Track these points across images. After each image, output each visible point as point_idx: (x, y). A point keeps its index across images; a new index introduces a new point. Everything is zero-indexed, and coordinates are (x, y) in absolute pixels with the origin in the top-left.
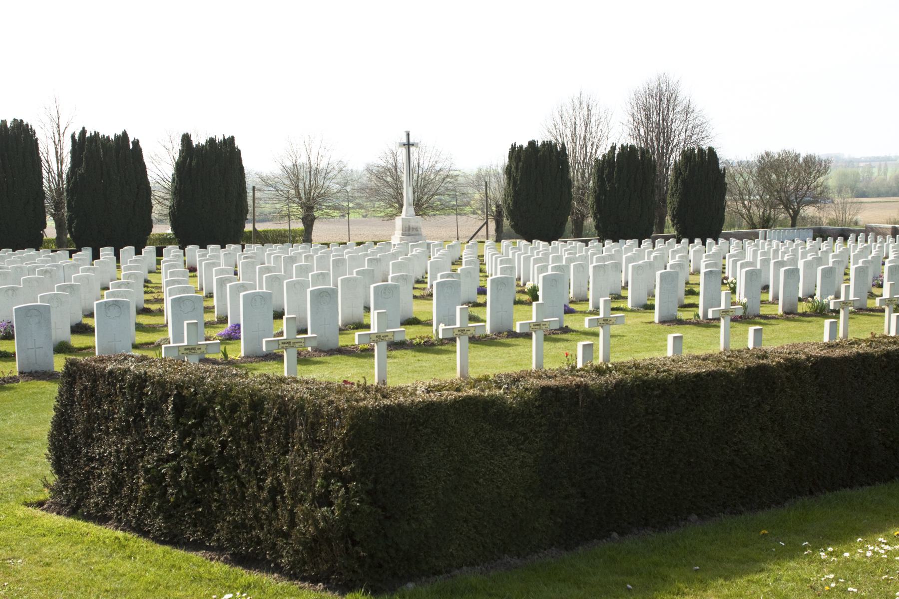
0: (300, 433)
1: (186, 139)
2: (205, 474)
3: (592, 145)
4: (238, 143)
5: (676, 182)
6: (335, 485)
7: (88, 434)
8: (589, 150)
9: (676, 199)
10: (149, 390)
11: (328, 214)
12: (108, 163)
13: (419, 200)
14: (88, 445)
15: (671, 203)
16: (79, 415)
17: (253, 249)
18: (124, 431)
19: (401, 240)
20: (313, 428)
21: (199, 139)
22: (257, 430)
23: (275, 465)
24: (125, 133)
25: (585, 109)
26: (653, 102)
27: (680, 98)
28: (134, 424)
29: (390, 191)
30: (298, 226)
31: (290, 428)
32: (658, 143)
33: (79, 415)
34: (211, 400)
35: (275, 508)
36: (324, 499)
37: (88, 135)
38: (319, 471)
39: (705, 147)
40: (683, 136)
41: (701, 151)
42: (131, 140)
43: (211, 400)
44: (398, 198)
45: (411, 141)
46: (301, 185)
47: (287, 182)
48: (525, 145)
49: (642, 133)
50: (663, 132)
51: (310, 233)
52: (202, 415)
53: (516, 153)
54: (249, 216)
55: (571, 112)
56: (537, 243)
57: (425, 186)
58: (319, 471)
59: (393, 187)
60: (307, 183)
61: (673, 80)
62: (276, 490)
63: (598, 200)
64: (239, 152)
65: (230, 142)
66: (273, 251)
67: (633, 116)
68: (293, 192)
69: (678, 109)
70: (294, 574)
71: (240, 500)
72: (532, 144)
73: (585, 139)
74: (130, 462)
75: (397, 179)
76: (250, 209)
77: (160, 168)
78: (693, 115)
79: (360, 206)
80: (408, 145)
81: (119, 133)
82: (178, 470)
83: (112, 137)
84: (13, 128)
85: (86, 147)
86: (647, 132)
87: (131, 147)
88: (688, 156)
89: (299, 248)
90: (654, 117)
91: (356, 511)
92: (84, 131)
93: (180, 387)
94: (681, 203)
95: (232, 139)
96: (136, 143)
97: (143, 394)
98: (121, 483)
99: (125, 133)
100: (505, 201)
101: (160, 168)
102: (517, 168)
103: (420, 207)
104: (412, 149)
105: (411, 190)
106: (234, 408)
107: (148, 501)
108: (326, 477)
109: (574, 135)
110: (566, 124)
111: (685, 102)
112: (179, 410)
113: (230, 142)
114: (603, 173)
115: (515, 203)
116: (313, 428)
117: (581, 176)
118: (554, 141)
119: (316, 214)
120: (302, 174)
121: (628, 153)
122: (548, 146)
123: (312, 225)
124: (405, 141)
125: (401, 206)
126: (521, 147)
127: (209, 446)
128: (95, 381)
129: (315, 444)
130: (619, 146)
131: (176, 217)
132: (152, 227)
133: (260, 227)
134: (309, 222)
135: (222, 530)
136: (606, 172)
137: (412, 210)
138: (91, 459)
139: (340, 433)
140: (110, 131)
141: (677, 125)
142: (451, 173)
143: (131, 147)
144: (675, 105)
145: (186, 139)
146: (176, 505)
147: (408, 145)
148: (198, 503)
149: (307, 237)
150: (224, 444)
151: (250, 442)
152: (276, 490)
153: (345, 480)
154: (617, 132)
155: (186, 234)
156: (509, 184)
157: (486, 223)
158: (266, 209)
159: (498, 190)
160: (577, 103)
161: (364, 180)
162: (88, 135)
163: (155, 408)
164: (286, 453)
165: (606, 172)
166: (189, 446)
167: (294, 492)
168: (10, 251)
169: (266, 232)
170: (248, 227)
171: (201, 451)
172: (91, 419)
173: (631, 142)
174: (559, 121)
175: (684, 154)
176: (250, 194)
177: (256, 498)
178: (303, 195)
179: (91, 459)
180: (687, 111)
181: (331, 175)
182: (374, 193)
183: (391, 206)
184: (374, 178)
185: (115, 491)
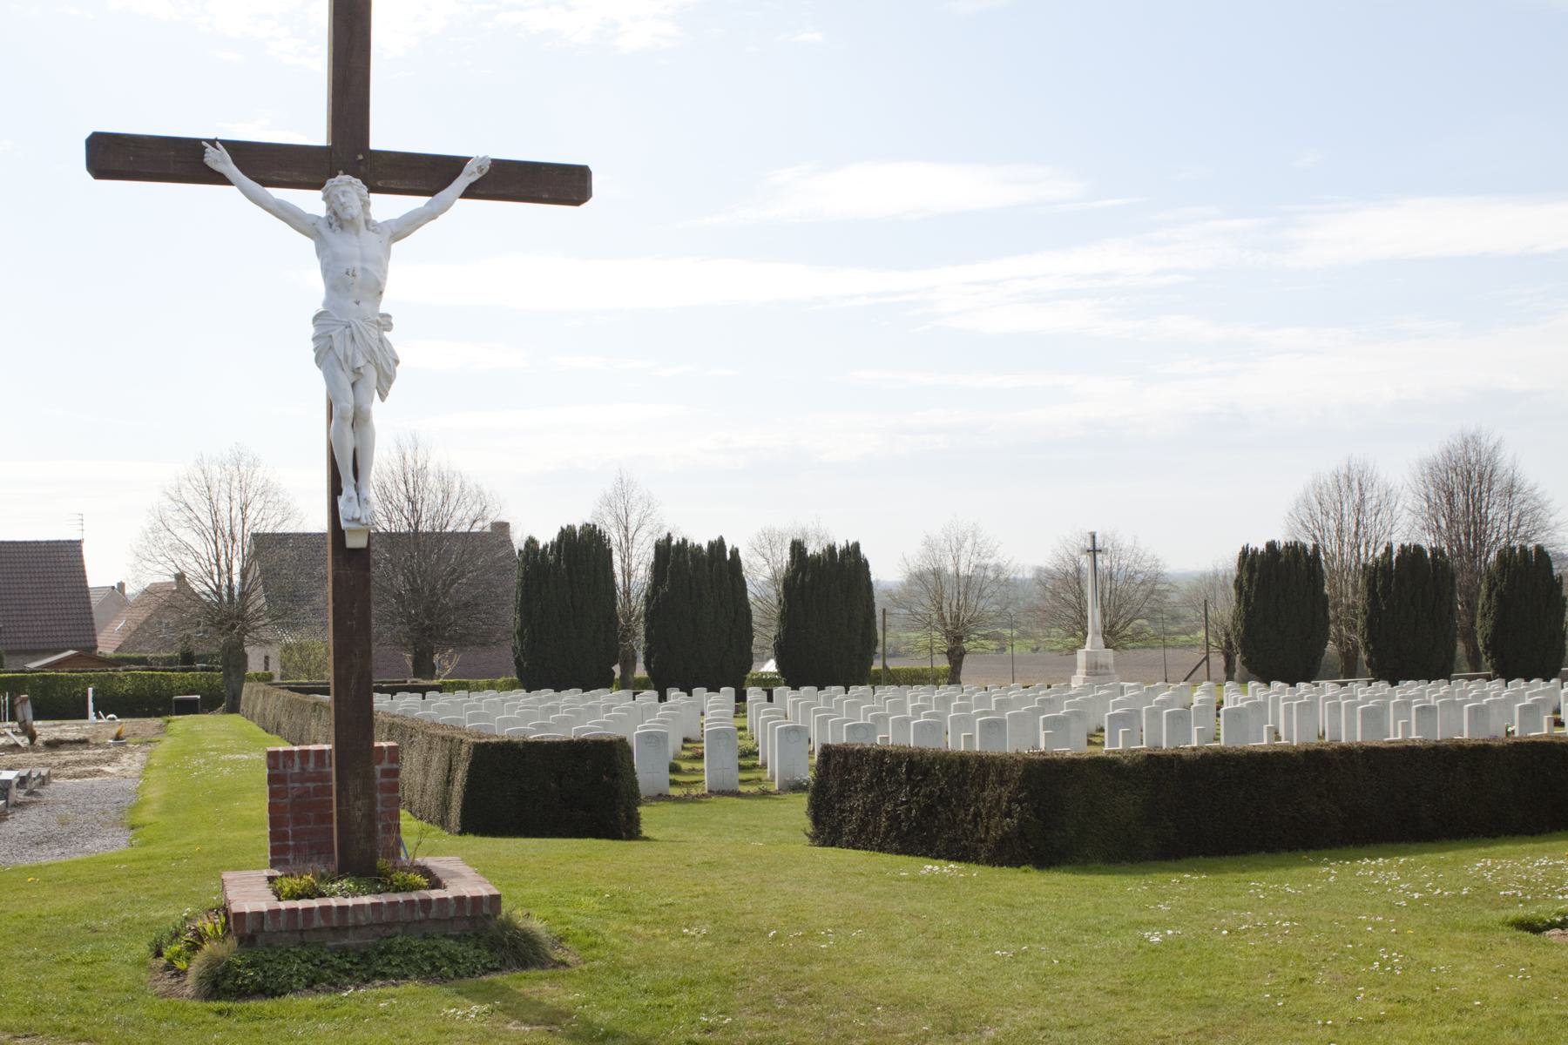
0: (993, 777)
1: (797, 548)
2: (928, 811)
3: (1367, 543)
4: (865, 551)
5: (1489, 596)
6: (1015, 806)
8: (1362, 550)
9: (1489, 622)
11: (983, 646)
12: (697, 578)
13: (1112, 626)
15: (639, 643)
16: (834, 784)
17: (887, 692)
19: (1085, 680)
20: (1001, 773)
21: (813, 549)
23: (977, 799)
25: (1356, 491)
26: (1457, 480)
27: (1499, 472)
29: (1070, 612)
30: (943, 664)
32: (1468, 540)
33: (834, 784)
34: (932, 764)
36: (1009, 814)
37: (674, 543)
38: (1005, 798)
39: (1531, 546)
40: (1504, 529)
41: (1523, 549)
42: (729, 549)
43: (932, 764)
46: (945, 605)
47: (927, 602)
48: (1262, 547)
49: (1443, 523)
50: (1476, 525)
52: (926, 773)
54: (879, 649)
56: (1277, 685)
57: (1121, 606)
58: (1005, 798)
60: (954, 603)
61: (1488, 443)
62: (977, 815)
63: (1370, 623)
64: (866, 564)
65: (853, 551)
66: (919, 692)
67: (1428, 499)
68: (935, 616)
69: (1496, 488)
72: (1271, 546)
74: (875, 810)
75: (1081, 595)
76: (880, 637)
78: (1518, 497)
79: (1025, 635)
80: (1094, 551)
81: (714, 538)
82: (909, 810)
83: (705, 547)
84: (582, 536)
85: (670, 556)
86: (1451, 522)
88: (1506, 557)
89: (945, 690)
90: (1460, 500)
92: (669, 538)
94: (1495, 627)
95: (857, 546)
96: (735, 553)
100: (1234, 626)
102: (1250, 580)
103: (1112, 636)
104: (1099, 556)
105: (1098, 612)
106: (949, 766)
108: (1009, 802)
109: (1340, 531)
110: (1327, 514)
112: (909, 772)
113: (853, 551)
114: (1375, 585)
116: (1001, 773)
117: (1345, 595)
118: (1310, 544)
119: (966, 646)
120: (948, 591)
121: (1412, 555)
122: (1295, 550)
123: (960, 662)
124: (1089, 546)
125: (1086, 634)
129: (1002, 783)
130: (1396, 548)
133: (893, 665)
134: (956, 657)
136: (1379, 584)
137: (1100, 641)
138: (843, 811)
139: (1017, 774)
140: (701, 538)
141: (1495, 512)
142: (1158, 587)
144: (1491, 483)
146: (908, 833)
147: (1094, 551)
149: (953, 677)
150: (942, 790)
153: (1020, 802)
154: (1406, 525)
155: (796, 673)
156: (1239, 602)
157: (1207, 658)
158: (902, 640)
159: (1226, 608)
160: (1343, 482)
162: (674, 543)
163: (892, 771)
164: (983, 790)
165: (1379, 584)
166: (917, 794)
168: (550, 692)
169: (898, 671)
170: (877, 665)
173: (1427, 541)
174: (1317, 507)
175: (1501, 555)
176: (879, 618)
178: (947, 615)
179: (843, 811)
180: (1510, 491)
181: (988, 591)
183: (1074, 635)
184: (1048, 594)
185: (861, 831)
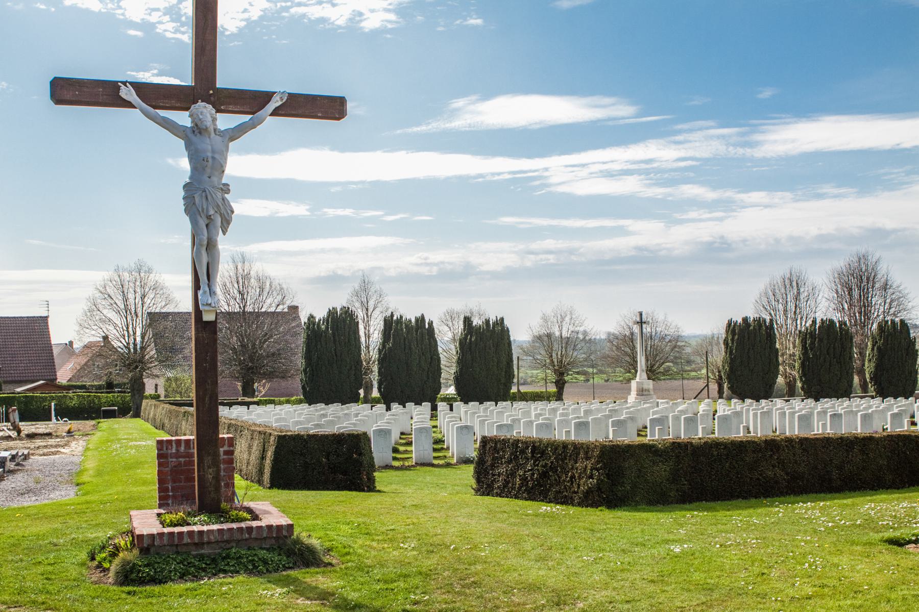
0: (582, 455)
1: (467, 321)
2: (544, 475)
3: (801, 318)
4: (507, 323)
6: (595, 472)
7: (492, 465)
9: (873, 365)
10: (520, 445)
13: (652, 367)
14: (493, 470)
18: (509, 462)
19: (636, 399)
20: (587, 453)
22: (565, 457)
23: (572, 468)
24: (423, 316)
25: (795, 287)
28: (514, 458)
29: (627, 358)
30: (553, 389)
31: (578, 454)
33: (489, 460)
34: (546, 447)
35: (572, 484)
36: (591, 477)
37: (395, 318)
38: (589, 467)
44: (633, 364)
45: (643, 320)
46: (554, 355)
48: (740, 320)
51: (562, 394)
52: (543, 453)
53: (731, 327)
54: (515, 380)
55: (783, 290)
57: (657, 355)
58: (589, 467)
59: (629, 356)
60: (559, 353)
61: (872, 259)
62: (573, 477)
63: (803, 365)
67: (837, 292)
68: (548, 361)
69: (877, 285)
70: (580, 505)
71: (558, 483)
72: (745, 320)
73: (795, 312)
74: (513, 474)
77: (447, 340)
78: (890, 291)
79: (601, 372)
81: (419, 315)
82: (533, 474)
84: (341, 314)
87: (427, 326)
89: (554, 404)
91: (602, 481)
93: (534, 442)
94: (876, 367)
97: (517, 447)
98: (508, 483)
99: (423, 316)
101: (447, 340)
102: (733, 340)
103: (652, 373)
106: (556, 449)
107: (520, 488)
108: (591, 470)
111: (883, 280)
115: (731, 368)
116: (587, 453)
119: (566, 378)
122: (759, 322)
123: (563, 388)
125: (636, 371)
126: (736, 323)
127: (546, 464)
128: (496, 444)
129: (587, 458)
130: (818, 321)
131: (460, 382)
132: (440, 388)
133: (523, 389)
134: (560, 384)
135: (551, 495)
136: (808, 342)
137: (645, 376)
138: (494, 475)
142: (679, 344)
143: (427, 326)
144: (874, 283)
145: (467, 321)
146: (532, 488)
147: (641, 323)
148: (541, 486)
149: (559, 397)
150: (552, 463)
151: (563, 461)
152: (573, 477)
153: (598, 470)
157: (707, 385)
158: (528, 374)
160: (787, 282)
161: (607, 351)
163: (523, 452)
165: (808, 342)
167: (579, 477)
169: (526, 393)
170: (514, 390)
171: (542, 466)
172: (494, 459)
176: (515, 362)
177: (564, 481)
178: (555, 360)
179: (494, 475)
180: (885, 287)
182: (616, 362)
183: (630, 372)
184: (614, 348)
185: (505, 487)
